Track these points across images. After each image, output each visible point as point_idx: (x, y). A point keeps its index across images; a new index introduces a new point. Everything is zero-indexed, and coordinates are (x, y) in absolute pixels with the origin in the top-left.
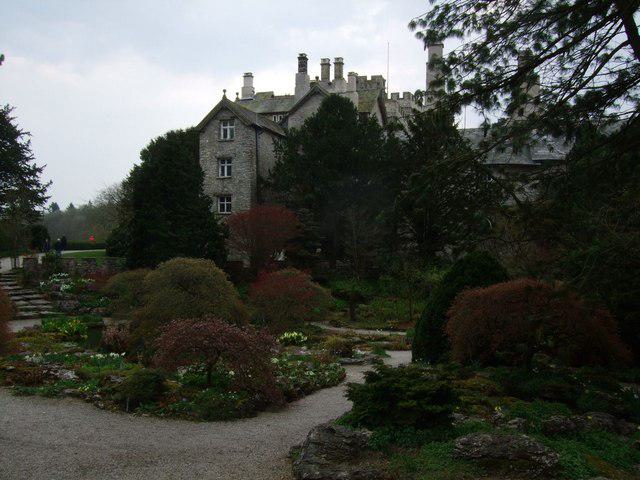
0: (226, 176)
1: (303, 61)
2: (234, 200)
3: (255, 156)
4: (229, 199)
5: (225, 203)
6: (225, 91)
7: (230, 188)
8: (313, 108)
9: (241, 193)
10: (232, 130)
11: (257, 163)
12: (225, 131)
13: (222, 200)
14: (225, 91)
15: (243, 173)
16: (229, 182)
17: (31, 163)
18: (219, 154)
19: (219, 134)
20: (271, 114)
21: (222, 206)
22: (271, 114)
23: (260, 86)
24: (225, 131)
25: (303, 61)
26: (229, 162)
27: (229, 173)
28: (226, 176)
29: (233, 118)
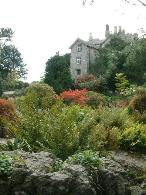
0: (79, 63)
1: (107, 27)
2: (81, 71)
3: (89, 57)
4: (80, 71)
5: (79, 72)
6: (140, 16)
7: (81, 67)
8: (109, 40)
9: (84, 69)
10: (81, 48)
11: (89, 59)
12: (79, 48)
13: (78, 71)
14: (140, 16)
15: (85, 62)
16: (78, 69)
17: (56, 55)
18: (77, 56)
19: (77, 49)
20: (97, 44)
21: (78, 73)
22: (97, 44)
23: (94, 37)
24: (79, 48)
25: (107, 27)
26: (80, 58)
27: (80, 62)
28: (79, 63)
29: (81, 44)
